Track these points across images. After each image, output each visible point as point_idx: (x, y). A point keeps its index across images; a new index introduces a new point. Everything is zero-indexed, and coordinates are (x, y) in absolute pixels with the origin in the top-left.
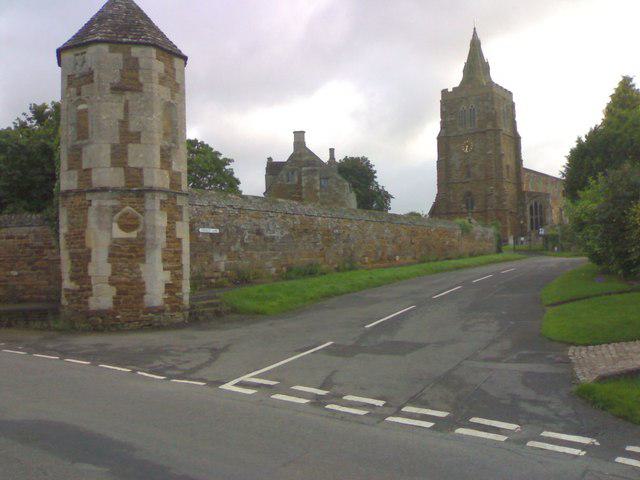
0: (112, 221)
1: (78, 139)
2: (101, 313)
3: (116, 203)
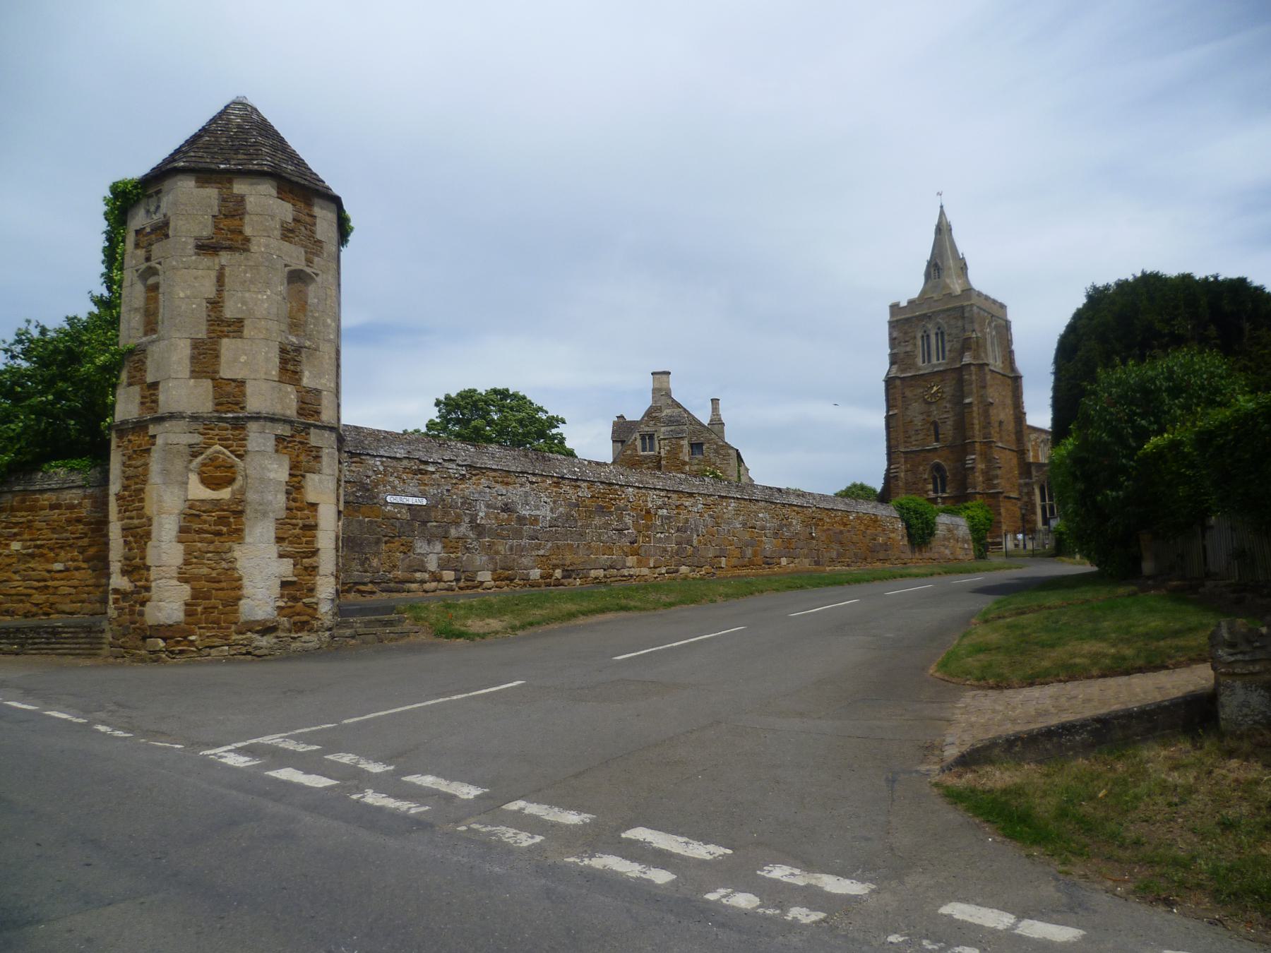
0: (188, 469)
1: (146, 334)
2: (166, 631)
3: (197, 439)
